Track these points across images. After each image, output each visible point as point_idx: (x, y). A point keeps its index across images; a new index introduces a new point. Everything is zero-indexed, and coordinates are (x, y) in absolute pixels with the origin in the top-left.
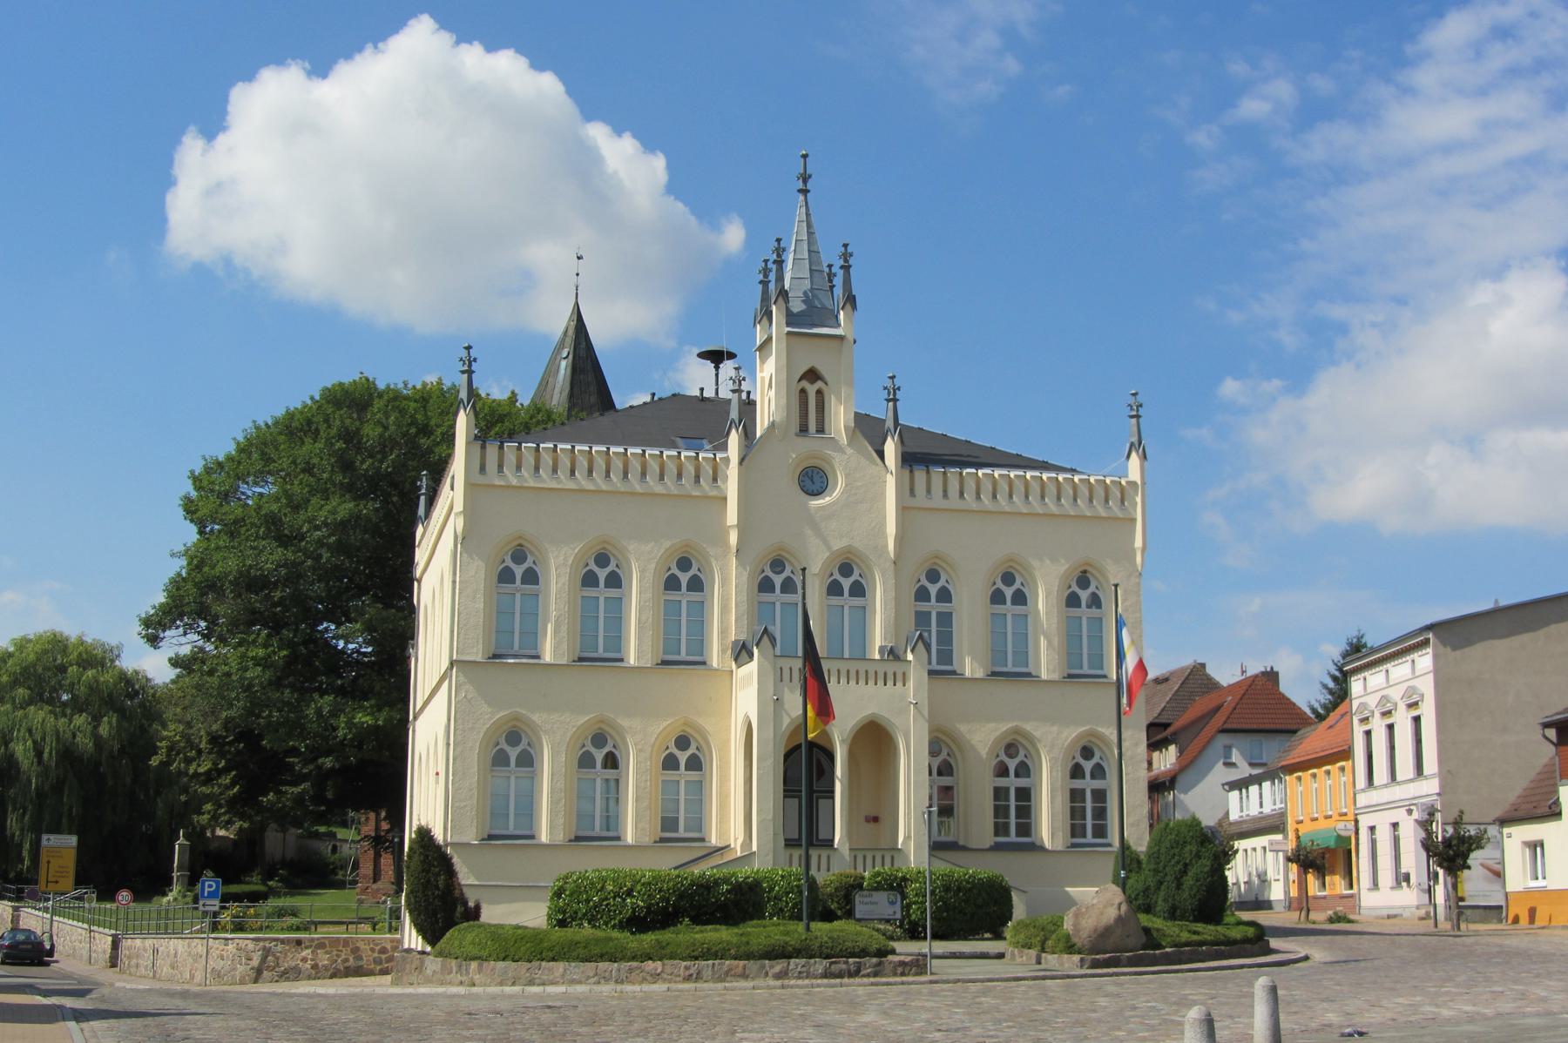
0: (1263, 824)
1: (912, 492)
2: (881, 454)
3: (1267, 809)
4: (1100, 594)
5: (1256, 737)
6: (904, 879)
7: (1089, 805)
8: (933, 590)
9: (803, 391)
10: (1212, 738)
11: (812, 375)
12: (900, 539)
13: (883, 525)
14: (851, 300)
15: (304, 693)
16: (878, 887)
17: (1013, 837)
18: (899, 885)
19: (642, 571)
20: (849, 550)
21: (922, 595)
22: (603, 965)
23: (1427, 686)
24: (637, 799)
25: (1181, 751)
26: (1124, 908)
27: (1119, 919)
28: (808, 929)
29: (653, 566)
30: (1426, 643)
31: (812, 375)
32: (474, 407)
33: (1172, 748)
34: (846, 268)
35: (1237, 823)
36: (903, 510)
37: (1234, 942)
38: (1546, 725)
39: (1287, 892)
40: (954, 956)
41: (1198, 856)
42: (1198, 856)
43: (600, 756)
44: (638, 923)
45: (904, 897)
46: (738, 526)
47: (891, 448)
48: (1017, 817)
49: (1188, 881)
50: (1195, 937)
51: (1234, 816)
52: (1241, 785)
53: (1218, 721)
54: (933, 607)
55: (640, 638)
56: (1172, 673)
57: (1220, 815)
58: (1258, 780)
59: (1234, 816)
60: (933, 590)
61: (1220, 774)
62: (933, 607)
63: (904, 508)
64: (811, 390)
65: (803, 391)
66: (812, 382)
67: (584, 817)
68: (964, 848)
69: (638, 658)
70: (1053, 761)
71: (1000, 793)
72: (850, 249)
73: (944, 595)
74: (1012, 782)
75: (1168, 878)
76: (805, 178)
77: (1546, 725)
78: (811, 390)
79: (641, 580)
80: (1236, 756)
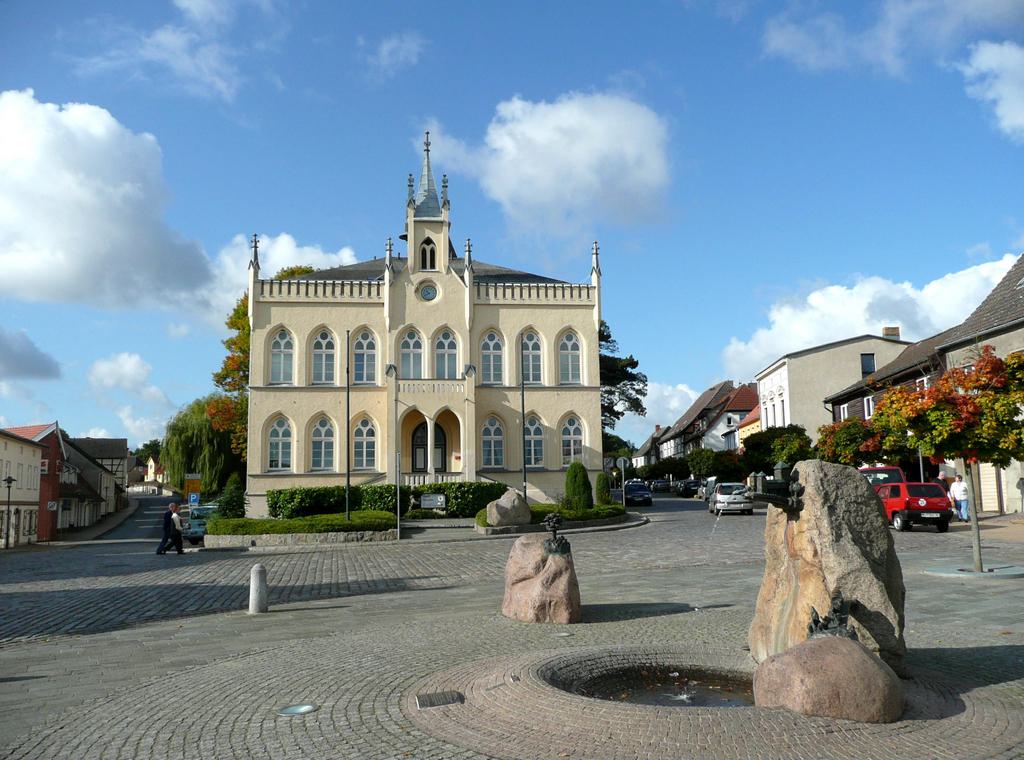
2: (462, 278)
4: (500, 343)
12: (472, 320)
14: (446, 203)
15: (910, 427)
17: (493, 466)
22: (332, 535)
23: (785, 384)
30: (784, 364)
32: (472, 268)
36: (474, 306)
38: (826, 402)
40: (582, 532)
44: (298, 512)
47: (466, 275)
48: (325, 448)
64: (428, 248)
65: (424, 252)
66: (428, 245)
68: (547, 471)
69: (299, 383)
71: (527, 444)
74: (493, 438)
76: (428, 144)
77: (826, 402)
78: (428, 248)
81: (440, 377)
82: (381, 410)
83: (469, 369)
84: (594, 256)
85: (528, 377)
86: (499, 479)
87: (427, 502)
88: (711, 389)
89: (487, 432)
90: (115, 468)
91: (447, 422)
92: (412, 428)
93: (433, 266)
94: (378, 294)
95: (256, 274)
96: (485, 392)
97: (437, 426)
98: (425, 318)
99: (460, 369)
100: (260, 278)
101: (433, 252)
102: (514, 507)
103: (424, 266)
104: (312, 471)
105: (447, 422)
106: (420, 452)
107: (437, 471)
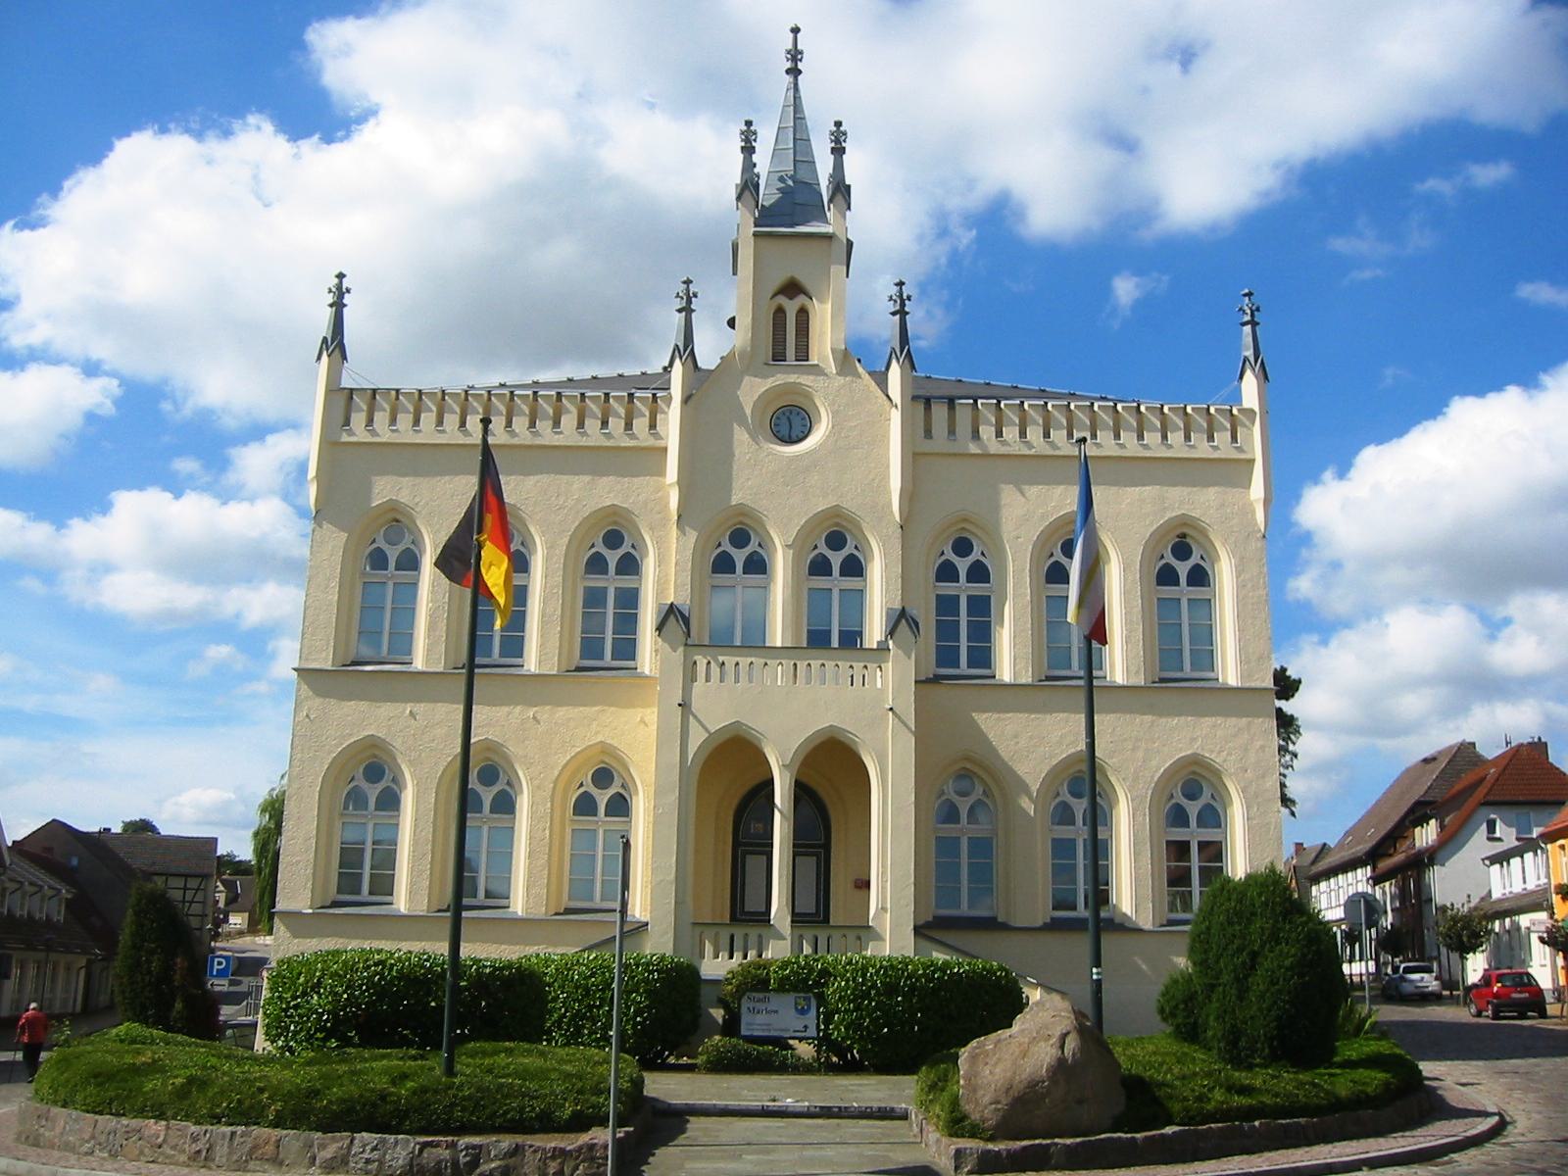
0: (1525, 902)
1: (928, 433)
3: (1531, 885)
5: (1524, 810)
6: (825, 973)
7: (1195, 862)
8: (963, 565)
9: (780, 312)
10: (1473, 811)
11: (792, 289)
12: (909, 496)
13: (886, 477)
16: (784, 985)
18: (817, 984)
19: (550, 547)
20: (835, 512)
21: (946, 572)
24: (531, 855)
25: (1442, 827)
26: (1071, 1044)
27: (1060, 1067)
28: (450, 1071)
29: (566, 540)
31: (792, 289)
33: (1433, 822)
34: (838, 151)
35: (1500, 901)
36: (914, 459)
37: (1337, 1105)
39: (1555, 979)
41: (1275, 938)
42: (1275, 938)
43: (478, 789)
45: (821, 999)
46: (679, 482)
49: (1258, 982)
50: (1238, 1100)
51: (1496, 895)
52: (1501, 858)
53: (1480, 793)
54: (963, 589)
55: (543, 635)
56: (1440, 752)
57: (1484, 893)
58: (1518, 852)
59: (1496, 895)
60: (963, 565)
61: (1478, 845)
62: (963, 589)
63: (915, 454)
64: (792, 307)
65: (780, 312)
67: (581, 883)
68: (1005, 927)
70: (1135, 800)
72: (346, 283)
73: (979, 573)
74: (965, 831)
75: (1225, 978)
78: (792, 307)
79: (547, 559)
80: (1500, 830)
81: (818, 639)
82: (643, 735)
83: (901, 620)
84: (1248, 329)
85: (1072, 670)
86: (990, 954)
87: (761, 1018)
88: (1426, 761)
89: (950, 814)
90: (189, 895)
91: (832, 775)
92: (731, 789)
93: (803, 353)
94: (653, 426)
95: (334, 375)
96: (941, 692)
97: (803, 792)
98: (783, 492)
99: (875, 631)
100: (347, 382)
101: (803, 314)
102: (1061, 1061)
103: (779, 356)
104: (336, 904)
105: (832, 775)
106: (754, 862)
107: (798, 919)
